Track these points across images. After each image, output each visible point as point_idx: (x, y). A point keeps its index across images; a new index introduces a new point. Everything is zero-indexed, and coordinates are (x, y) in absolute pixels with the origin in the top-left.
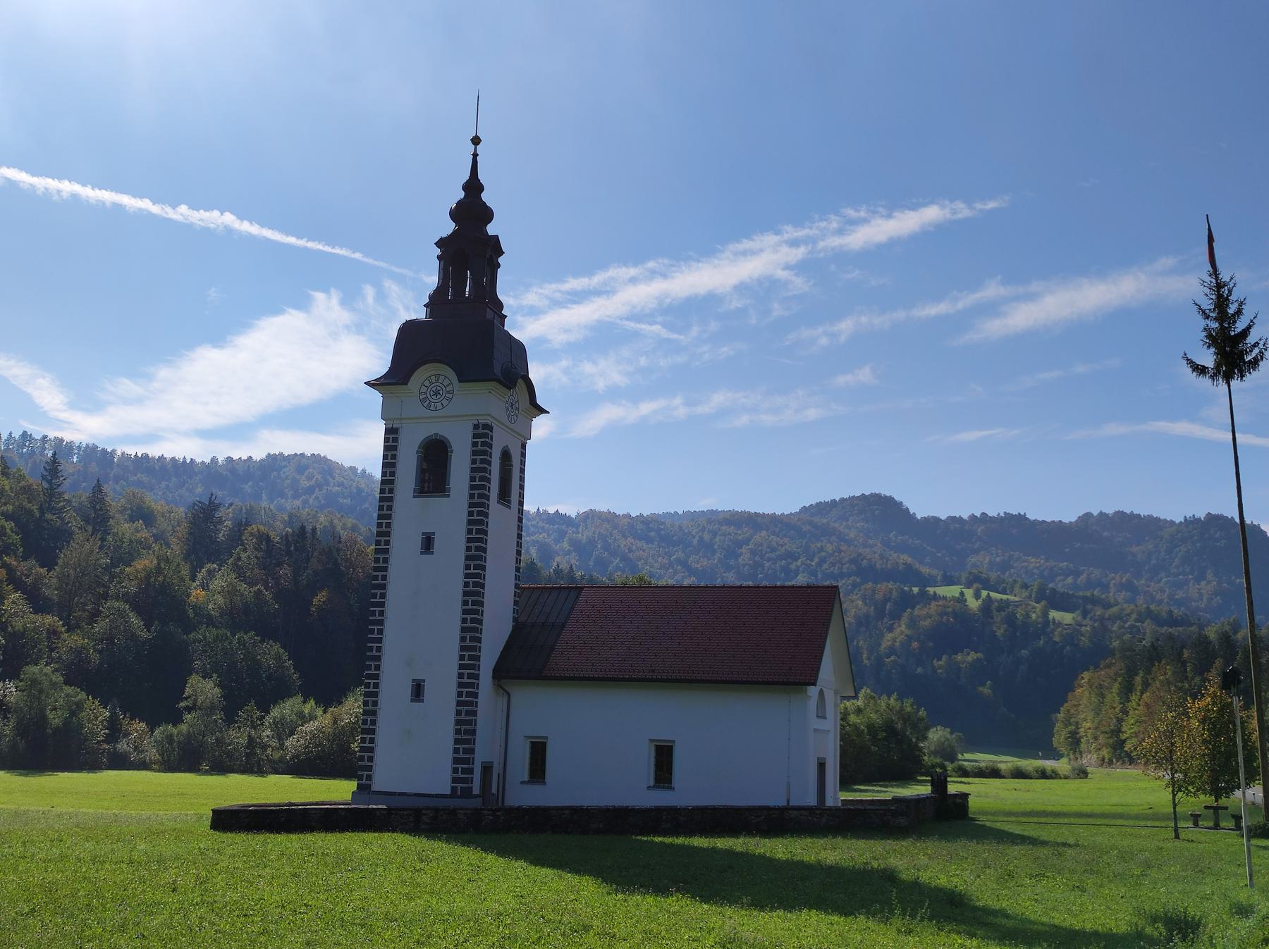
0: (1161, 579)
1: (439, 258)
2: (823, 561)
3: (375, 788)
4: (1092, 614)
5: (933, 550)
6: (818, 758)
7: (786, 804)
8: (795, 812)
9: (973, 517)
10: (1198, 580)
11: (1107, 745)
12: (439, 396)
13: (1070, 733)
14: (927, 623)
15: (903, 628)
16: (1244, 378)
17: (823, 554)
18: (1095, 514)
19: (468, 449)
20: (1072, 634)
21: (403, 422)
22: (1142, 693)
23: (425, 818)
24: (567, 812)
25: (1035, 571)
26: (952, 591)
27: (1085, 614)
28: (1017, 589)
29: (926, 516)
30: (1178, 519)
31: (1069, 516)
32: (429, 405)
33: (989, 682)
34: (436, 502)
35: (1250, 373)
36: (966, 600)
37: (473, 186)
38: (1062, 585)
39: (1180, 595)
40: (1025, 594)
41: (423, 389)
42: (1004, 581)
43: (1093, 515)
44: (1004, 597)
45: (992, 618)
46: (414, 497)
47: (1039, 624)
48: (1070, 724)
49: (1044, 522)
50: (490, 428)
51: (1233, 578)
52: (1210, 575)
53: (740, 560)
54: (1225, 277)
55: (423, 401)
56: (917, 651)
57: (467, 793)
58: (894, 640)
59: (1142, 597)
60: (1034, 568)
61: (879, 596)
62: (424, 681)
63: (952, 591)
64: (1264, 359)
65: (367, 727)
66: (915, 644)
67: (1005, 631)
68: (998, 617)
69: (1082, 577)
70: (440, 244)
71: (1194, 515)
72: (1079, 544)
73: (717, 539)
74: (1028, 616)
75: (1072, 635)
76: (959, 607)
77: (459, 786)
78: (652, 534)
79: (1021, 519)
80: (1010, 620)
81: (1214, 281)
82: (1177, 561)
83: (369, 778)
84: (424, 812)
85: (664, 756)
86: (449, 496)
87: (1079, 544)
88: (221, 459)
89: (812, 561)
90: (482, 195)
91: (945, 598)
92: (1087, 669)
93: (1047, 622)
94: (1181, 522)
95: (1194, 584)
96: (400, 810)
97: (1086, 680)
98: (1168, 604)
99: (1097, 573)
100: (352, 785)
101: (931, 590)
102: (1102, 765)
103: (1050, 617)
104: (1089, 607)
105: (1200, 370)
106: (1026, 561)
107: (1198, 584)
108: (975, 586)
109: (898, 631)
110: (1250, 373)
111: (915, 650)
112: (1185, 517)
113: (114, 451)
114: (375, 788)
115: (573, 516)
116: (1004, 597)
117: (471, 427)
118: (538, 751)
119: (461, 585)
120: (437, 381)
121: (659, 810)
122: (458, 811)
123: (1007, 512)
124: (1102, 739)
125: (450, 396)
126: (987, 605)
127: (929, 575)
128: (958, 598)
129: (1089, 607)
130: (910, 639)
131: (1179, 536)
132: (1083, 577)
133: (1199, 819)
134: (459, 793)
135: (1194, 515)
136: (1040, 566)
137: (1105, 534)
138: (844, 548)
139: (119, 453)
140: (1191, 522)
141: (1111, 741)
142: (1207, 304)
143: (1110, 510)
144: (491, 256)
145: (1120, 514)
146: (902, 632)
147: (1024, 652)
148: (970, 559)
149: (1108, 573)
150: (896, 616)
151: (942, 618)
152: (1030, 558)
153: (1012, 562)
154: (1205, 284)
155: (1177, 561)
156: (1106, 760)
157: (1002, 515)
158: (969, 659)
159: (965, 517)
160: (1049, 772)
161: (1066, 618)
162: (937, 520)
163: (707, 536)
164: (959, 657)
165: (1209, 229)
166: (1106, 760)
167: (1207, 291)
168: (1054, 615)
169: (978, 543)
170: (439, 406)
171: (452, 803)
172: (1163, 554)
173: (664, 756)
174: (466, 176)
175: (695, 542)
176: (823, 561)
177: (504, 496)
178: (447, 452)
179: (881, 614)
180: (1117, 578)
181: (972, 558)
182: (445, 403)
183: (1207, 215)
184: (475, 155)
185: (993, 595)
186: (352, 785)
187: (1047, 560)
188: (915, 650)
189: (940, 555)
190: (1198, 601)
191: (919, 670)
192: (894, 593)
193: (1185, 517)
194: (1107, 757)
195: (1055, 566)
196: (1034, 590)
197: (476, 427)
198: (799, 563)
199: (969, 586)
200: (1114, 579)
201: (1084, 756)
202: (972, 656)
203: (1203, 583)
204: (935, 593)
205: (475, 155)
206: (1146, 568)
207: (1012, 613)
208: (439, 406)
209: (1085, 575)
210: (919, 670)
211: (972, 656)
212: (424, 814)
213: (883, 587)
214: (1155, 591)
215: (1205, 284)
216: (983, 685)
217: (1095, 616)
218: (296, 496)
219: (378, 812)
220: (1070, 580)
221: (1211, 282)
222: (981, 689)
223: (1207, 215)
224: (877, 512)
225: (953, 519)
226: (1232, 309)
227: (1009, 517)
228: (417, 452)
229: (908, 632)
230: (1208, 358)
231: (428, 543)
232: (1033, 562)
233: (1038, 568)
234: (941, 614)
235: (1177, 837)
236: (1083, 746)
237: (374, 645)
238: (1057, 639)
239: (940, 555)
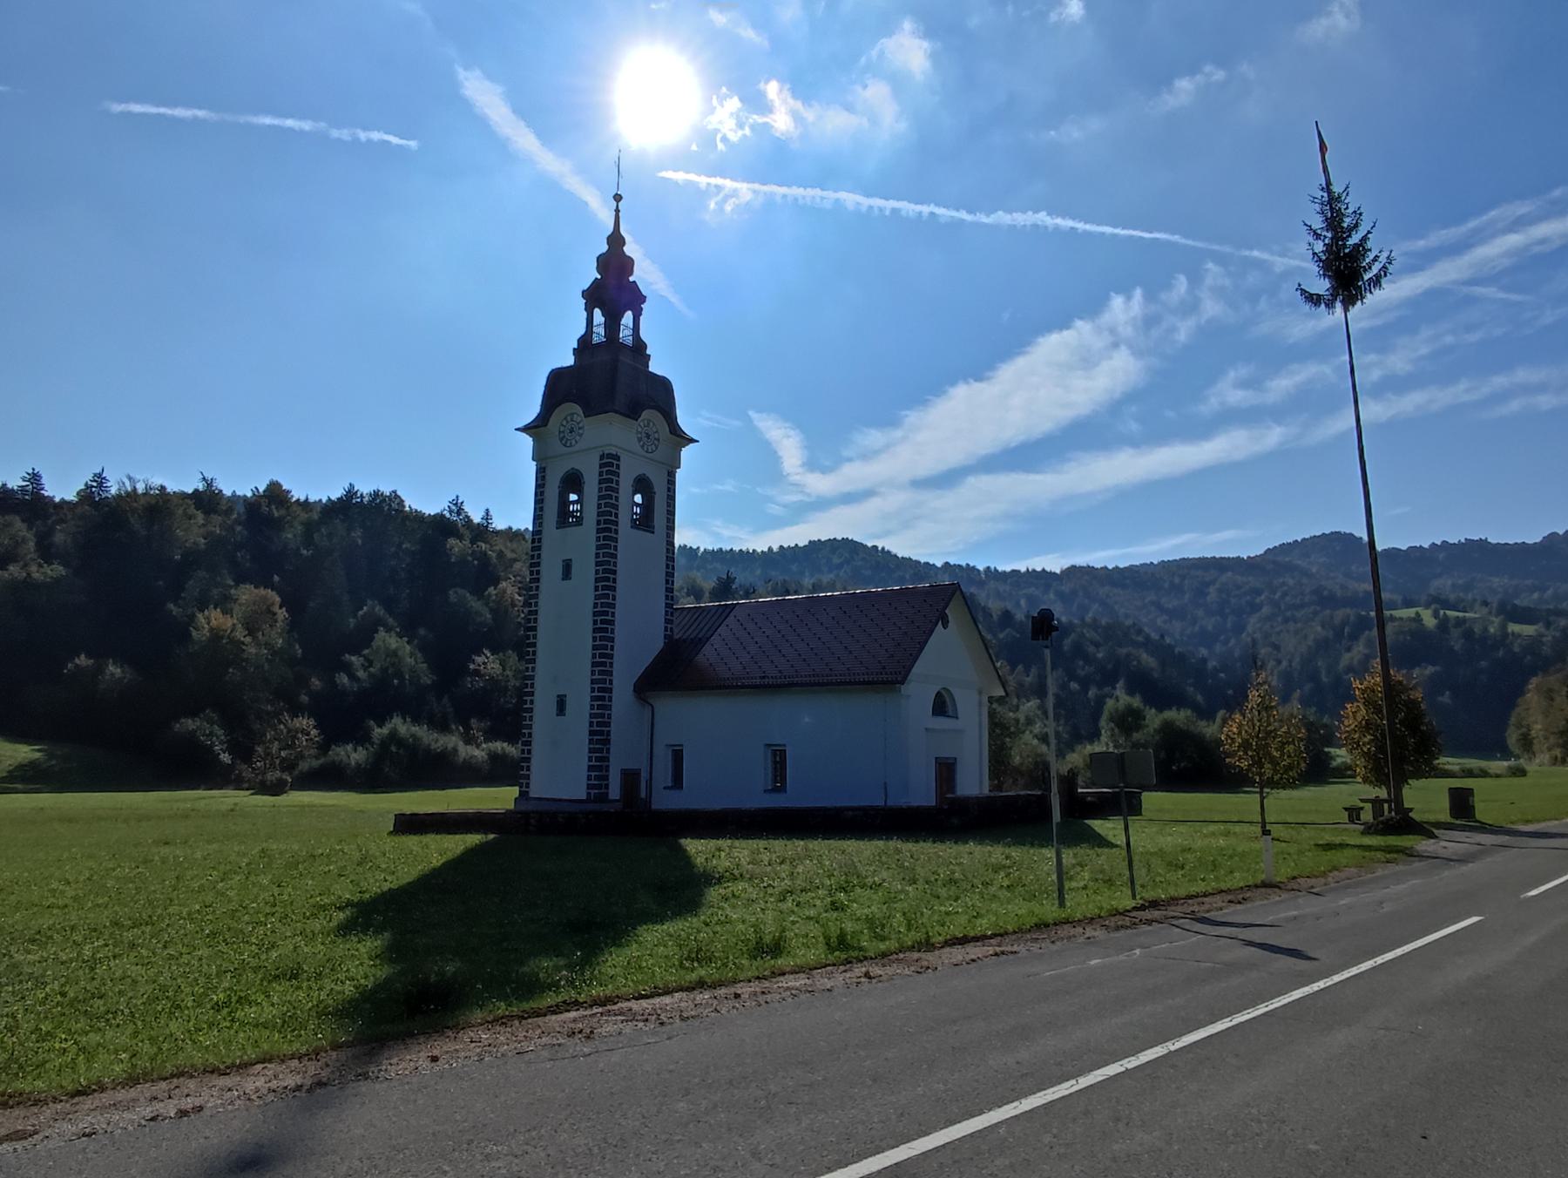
2: (1285, 594)
3: (532, 795)
6: (936, 758)
8: (850, 813)
11: (1558, 746)
13: (1522, 734)
15: (1361, 648)
16: (1364, 300)
17: (1285, 588)
19: (596, 478)
26: (1409, 612)
27: (1548, 625)
28: (1477, 606)
31: (1534, 537)
35: (1371, 292)
36: (1422, 620)
38: (1523, 601)
40: (1485, 610)
44: (1461, 614)
46: (557, 528)
48: (1522, 726)
50: (618, 458)
53: (1208, 598)
54: (1337, 188)
57: (603, 798)
58: (1352, 659)
61: (1337, 621)
62: (558, 715)
63: (1409, 612)
64: (1388, 274)
68: (1455, 633)
73: (1186, 582)
74: (1486, 630)
75: (1534, 644)
76: (1417, 630)
77: (593, 792)
78: (1128, 581)
80: (1468, 635)
81: (1325, 195)
83: (528, 785)
88: (775, 549)
89: (1275, 594)
90: (625, 248)
91: (1401, 619)
92: (1536, 675)
93: (1505, 635)
97: (1534, 685)
100: (514, 791)
102: (1554, 764)
103: (1510, 630)
104: (1551, 618)
105: (1314, 299)
108: (1433, 606)
109: (1355, 651)
110: (1371, 292)
113: (698, 548)
114: (532, 795)
115: (1058, 571)
116: (1461, 614)
124: (1552, 740)
126: (1444, 625)
132: (1550, 592)
133: (1361, 812)
138: (1305, 581)
139: (702, 549)
141: (1561, 741)
142: (1318, 223)
146: (1359, 652)
147: (1483, 664)
150: (1354, 637)
154: (1316, 200)
156: (1559, 759)
157: (1463, 541)
159: (1426, 546)
160: (1476, 772)
161: (1528, 630)
163: (1177, 580)
166: (1559, 759)
168: (1513, 628)
171: (591, 807)
175: (1166, 585)
176: (1285, 594)
177: (644, 522)
179: (1339, 634)
183: (1316, 122)
184: (617, 211)
185: (1448, 612)
186: (514, 791)
192: (1352, 618)
194: (1559, 756)
197: (602, 457)
198: (1263, 597)
199: (1427, 606)
201: (1537, 755)
202: (1430, 670)
204: (1391, 615)
205: (617, 211)
213: (1340, 614)
215: (1316, 200)
218: (830, 571)
220: (1536, 596)
221: (1322, 197)
222: (1440, 699)
223: (1316, 122)
224: (1338, 548)
226: (1347, 222)
229: (1366, 651)
230: (1322, 286)
236: (1536, 747)
238: (1517, 649)
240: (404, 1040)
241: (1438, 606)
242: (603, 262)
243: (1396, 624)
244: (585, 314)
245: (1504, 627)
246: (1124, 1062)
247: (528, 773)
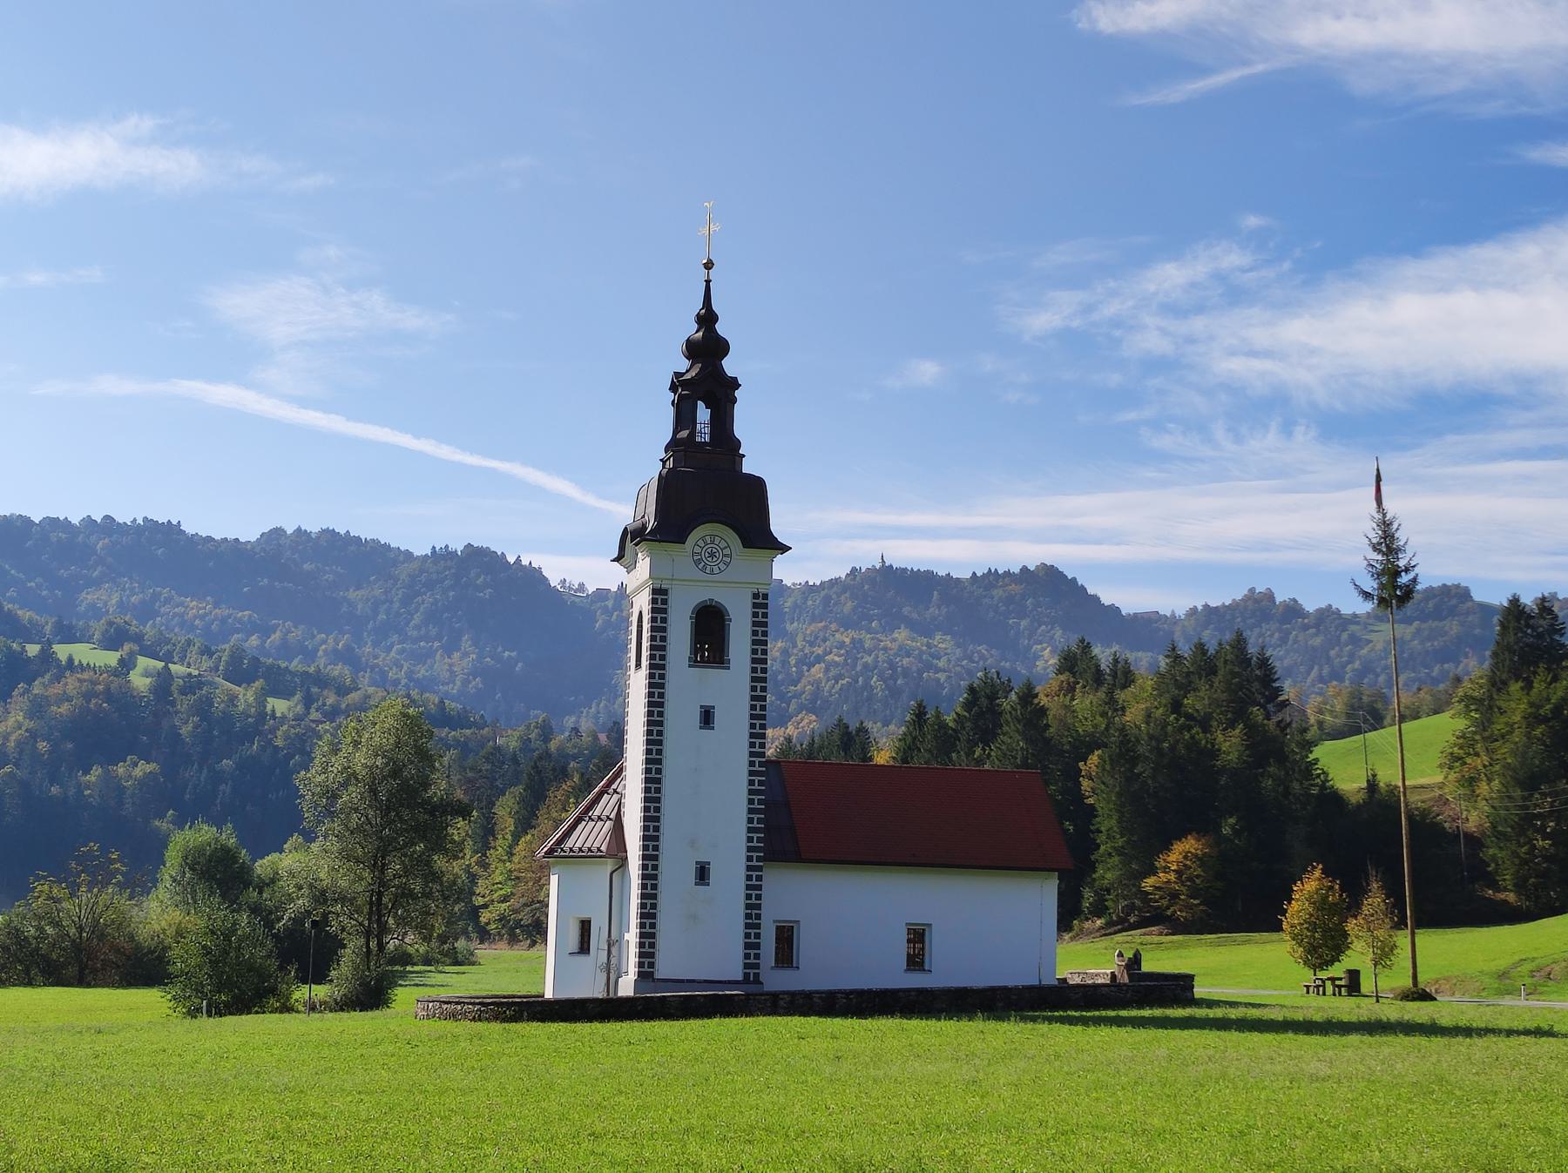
0: (392, 645)
3: (657, 976)
4: (320, 703)
5: (23, 576)
7: (1038, 983)
8: (1106, 989)
9: (88, 521)
10: (449, 652)
12: (715, 559)
14: (64, 708)
18: (289, 531)
19: (749, 620)
20: (304, 734)
21: (674, 582)
22: (517, 837)
23: (782, 1003)
24: (913, 993)
25: (197, 622)
28: (193, 654)
29: (8, 515)
30: (421, 549)
31: (249, 533)
33: (171, 812)
34: (713, 674)
37: (707, 318)
39: (422, 672)
40: (207, 663)
42: (168, 641)
43: (285, 532)
45: (173, 704)
47: (250, 716)
49: (210, 539)
51: (500, 649)
52: (466, 643)
55: (697, 563)
56: (46, 756)
59: (367, 675)
60: (195, 617)
62: (709, 863)
65: (647, 911)
66: (43, 746)
67: (196, 727)
68: (184, 704)
69: (273, 637)
71: (447, 546)
72: (266, 581)
79: (171, 531)
80: (203, 709)
82: (417, 619)
84: (781, 996)
85: (917, 936)
87: (266, 581)
93: (262, 716)
94: (427, 555)
95: (442, 656)
96: (756, 995)
98: (406, 685)
99: (297, 634)
101: (62, 651)
103: (269, 708)
104: (315, 690)
106: (182, 604)
107: (449, 657)
111: (43, 755)
112: (434, 547)
114: (657, 976)
117: (750, 596)
118: (786, 936)
120: (712, 543)
121: (921, 992)
122: (814, 995)
123: (150, 518)
127: (30, 621)
128: (116, 669)
129: (315, 690)
130: (33, 735)
131: (423, 578)
132: (276, 636)
134: (752, 979)
135: (447, 546)
136: (206, 615)
137: (306, 566)
140: (441, 557)
143: (313, 527)
145: (329, 534)
147: (227, 763)
148: (84, 594)
149: (315, 632)
151: (89, 702)
152: (188, 599)
153: (157, 604)
155: (417, 619)
158: (138, 772)
159: (75, 520)
162: (27, 521)
164: (121, 769)
165: (1378, 470)
167: (1375, 525)
169: (99, 568)
172: (397, 605)
173: (917, 936)
174: (697, 305)
178: (724, 620)
180: (330, 641)
181: (88, 593)
182: (722, 566)
184: (708, 282)
187: (216, 605)
188: (43, 755)
189: (33, 584)
190: (448, 684)
191: (55, 790)
193: (434, 547)
195: (229, 616)
196: (223, 659)
200: (324, 642)
202: (143, 769)
203: (456, 655)
204: (70, 660)
205: (708, 282)
206: (369, 627)
207: (207, 698)
209: (278, 634)
210: (55, 790)
211: (143, 769)
212: (782, 999)
214: (387, 665)
216: (162, 816)
217: (324, 704)
219: (698, 998)
225: (52, 523)
227: (151, 526)
229: (28, 724)
231: (707, 717)
232: (194, 607)
233: (202, 617)
234: (88, 696)
235: (1378, 1001)
238: (279, 743)
239: (33, 584)
240: (1111, 1025)
241: (136, 648)
242: (693, 350)
243: (86, 676)
244: (739, 430)
245: (261, 703)
246: (1127, 1015)
247: (651, 950)
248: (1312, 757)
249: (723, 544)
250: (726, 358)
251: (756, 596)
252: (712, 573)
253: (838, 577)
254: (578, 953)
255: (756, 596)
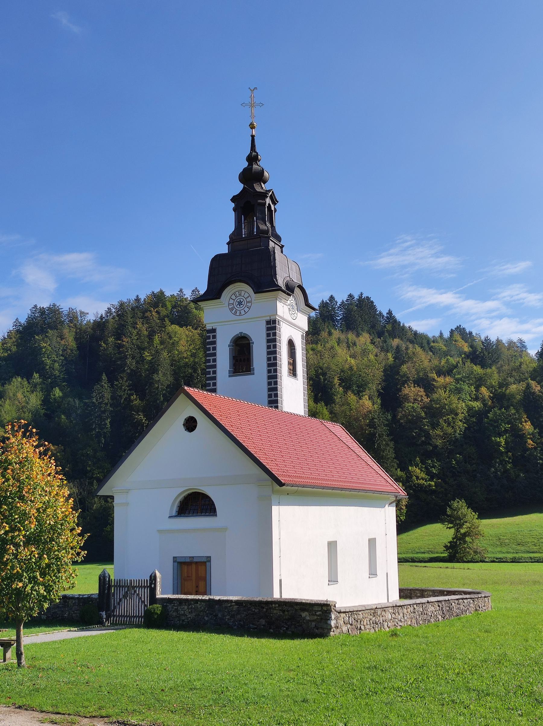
1: (234, 210)
32: (236, 312)
37: (253, 158)
41: (231, 301)
55: (231, 310)
70: (234, 199)
86: (253, 374)
112: (362, 294)
119: (266, 360)
125: (249, 304)
144: (269, 204)
170: (243, 312)
182: (246, 309)
193: (362, 294)
205: (253, 137)
208: (243, 312)
228: (229, 346)
237: (211, 346)
248: (468, 332)
249: (246, 295)
250: (488, 520)
251: (268, 322)
252: (240, 314)
253: (326, 299)
254: (175, 516)
255: (268, 322)
